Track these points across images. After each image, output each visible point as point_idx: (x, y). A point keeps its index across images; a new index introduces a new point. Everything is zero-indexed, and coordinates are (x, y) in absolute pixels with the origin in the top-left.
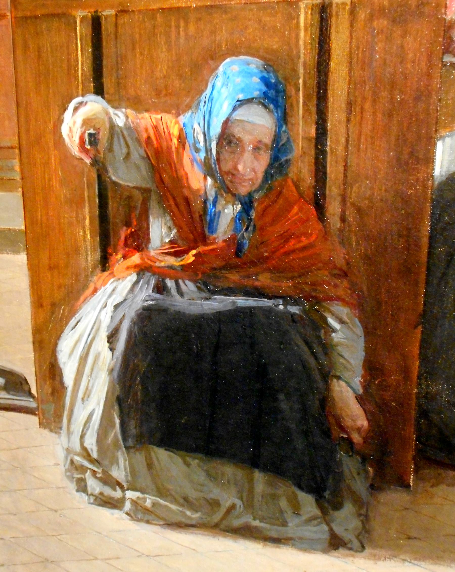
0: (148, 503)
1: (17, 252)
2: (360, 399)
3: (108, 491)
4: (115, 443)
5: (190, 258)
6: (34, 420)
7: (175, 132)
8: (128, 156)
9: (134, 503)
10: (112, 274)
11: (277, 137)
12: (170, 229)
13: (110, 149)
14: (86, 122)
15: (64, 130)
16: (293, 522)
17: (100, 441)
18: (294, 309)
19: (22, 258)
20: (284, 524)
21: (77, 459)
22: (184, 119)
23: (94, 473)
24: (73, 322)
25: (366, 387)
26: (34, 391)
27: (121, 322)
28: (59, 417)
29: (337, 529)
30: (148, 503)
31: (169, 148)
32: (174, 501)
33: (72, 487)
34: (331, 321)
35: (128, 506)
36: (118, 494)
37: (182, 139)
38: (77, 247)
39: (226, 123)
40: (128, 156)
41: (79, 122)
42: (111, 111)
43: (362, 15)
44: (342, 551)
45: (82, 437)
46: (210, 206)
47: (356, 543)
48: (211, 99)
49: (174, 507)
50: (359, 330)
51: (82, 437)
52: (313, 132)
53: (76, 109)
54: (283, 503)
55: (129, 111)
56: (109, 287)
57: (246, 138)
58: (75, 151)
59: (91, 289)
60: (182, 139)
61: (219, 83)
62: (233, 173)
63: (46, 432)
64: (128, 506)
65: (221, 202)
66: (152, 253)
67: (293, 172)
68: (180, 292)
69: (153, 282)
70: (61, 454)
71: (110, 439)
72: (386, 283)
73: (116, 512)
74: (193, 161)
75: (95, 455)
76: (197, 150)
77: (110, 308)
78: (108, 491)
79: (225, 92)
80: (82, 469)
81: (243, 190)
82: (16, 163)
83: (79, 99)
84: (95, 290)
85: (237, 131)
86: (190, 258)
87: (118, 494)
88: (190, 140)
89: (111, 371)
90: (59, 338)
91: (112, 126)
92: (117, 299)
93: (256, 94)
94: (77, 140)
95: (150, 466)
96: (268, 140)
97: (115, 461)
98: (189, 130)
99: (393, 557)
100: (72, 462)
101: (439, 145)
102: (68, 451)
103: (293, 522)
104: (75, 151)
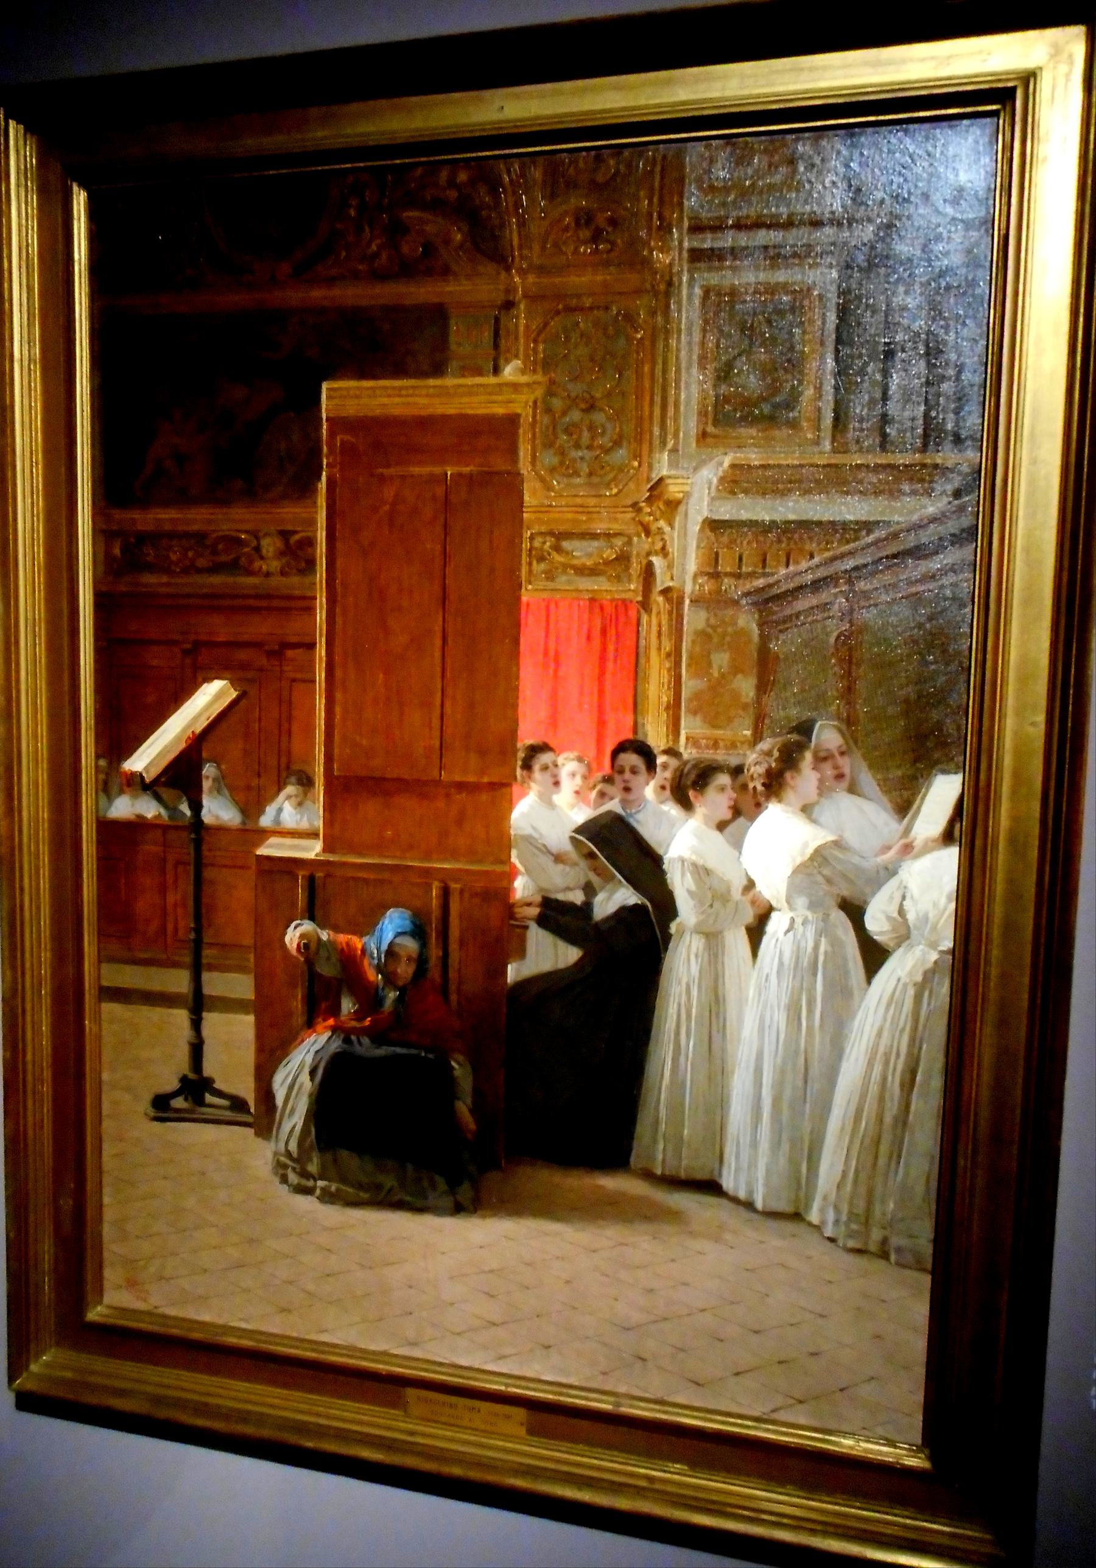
0: (333, 1188)
1: (247, 1013)
2: (471, 1111)
3: (304, 1182)
4: (311, 1147)
5: (367, 1022)
6: (250, 1132)
7: (359, 946)
8: (328, 958)
9: (323, 1189)
10: (315, 1031)
11: (420, 955)
12: (354, 1005)
13: (317, 953)
14: (302, 936)
15: (287, 939)
16: (431, 1196)
17: (300, 1144)
18: (431, 1056)
19: (250, 1019)
20: (426, 1198)
21: (282, 1159)
22: (365, 939)
23: (294, 1169)
24: (284, 1063)
25: (474, 1103)
26: (252, 1110)
27: (319, 1062)
28: (269, 1130)
29: (459, 1198)
30: (333, 1188)
31: (355, 956)
32: (352, 1186)
33: (277, 1180)
34: (453, 1064)
35: (318, 1192)
36: (311, 1183)
37: (363, 951)
38: (342, 949)
39: (391, 945)
40: (328, 958)
41: (298, 934)
42: (319, 930)
43: (466, 895)
44: (462, 1214)
45: (287, 1143)
46: (380, 991)
47: (471, 1208)
48: (381, 929)
49: (350, 1190)
50: (469, 1069)
51: (287, 1143)
52: (441, 954)
53: (295, 928)
54: (426, 1184)
55: (331, 933)
56: (313, 1038)
57: (403, 953)
58: (294, 952)
59: (299, 1040)
60: (363, 951)
61: (386, 922)
62: (395, 973)
63: (259, 1140)
64: (318, 1192)
65: (387, 990)
66: (343, 1018)
67: (430, 975)
68: (360, 1043)
69: (342, 1036)
70: (269, 1155)
71: (308, 1141)
72: (615, 472)
73: (309, 1198)
74: (370, 964)
75: (295, 1155)
76: (373, 958)
77: (312, 1053)
78: (304, 1182)
79: (390, 927)
80: (285, 1166)
81: (400, 983)
82: (252, 957)
83: (298, 922)
84: (303, 1041)
85: (397, 949)
86: (367, 1022)
87: (311, 1183)
88: (368, 952)
89: (310, 1095)
90: (274, 1072)
91: (319, 940)
92: (317, 1047)
93: (408, 929)
94: (295, 945)
95: (335, 1161)
96: (415, 955)
97: (310, 1160)
98: (368, 946)
99: (494, 1215)
100: (278, 1162)
101: (509, 967)
102: (276, 1154)
103: (431, 1196)
104: (294, 952)
